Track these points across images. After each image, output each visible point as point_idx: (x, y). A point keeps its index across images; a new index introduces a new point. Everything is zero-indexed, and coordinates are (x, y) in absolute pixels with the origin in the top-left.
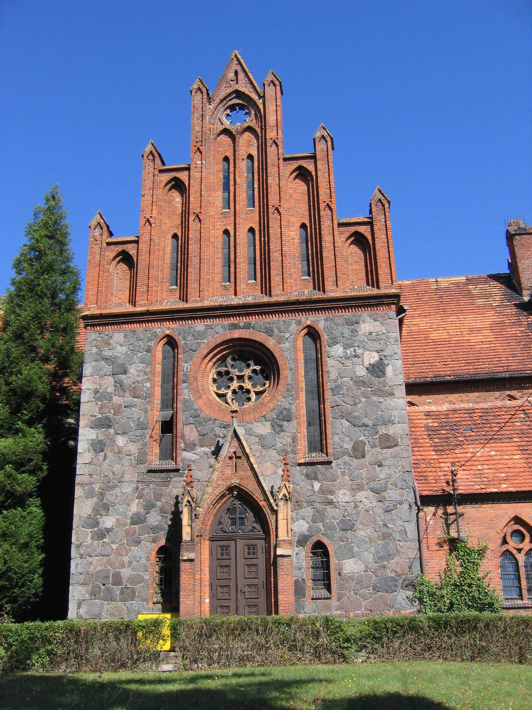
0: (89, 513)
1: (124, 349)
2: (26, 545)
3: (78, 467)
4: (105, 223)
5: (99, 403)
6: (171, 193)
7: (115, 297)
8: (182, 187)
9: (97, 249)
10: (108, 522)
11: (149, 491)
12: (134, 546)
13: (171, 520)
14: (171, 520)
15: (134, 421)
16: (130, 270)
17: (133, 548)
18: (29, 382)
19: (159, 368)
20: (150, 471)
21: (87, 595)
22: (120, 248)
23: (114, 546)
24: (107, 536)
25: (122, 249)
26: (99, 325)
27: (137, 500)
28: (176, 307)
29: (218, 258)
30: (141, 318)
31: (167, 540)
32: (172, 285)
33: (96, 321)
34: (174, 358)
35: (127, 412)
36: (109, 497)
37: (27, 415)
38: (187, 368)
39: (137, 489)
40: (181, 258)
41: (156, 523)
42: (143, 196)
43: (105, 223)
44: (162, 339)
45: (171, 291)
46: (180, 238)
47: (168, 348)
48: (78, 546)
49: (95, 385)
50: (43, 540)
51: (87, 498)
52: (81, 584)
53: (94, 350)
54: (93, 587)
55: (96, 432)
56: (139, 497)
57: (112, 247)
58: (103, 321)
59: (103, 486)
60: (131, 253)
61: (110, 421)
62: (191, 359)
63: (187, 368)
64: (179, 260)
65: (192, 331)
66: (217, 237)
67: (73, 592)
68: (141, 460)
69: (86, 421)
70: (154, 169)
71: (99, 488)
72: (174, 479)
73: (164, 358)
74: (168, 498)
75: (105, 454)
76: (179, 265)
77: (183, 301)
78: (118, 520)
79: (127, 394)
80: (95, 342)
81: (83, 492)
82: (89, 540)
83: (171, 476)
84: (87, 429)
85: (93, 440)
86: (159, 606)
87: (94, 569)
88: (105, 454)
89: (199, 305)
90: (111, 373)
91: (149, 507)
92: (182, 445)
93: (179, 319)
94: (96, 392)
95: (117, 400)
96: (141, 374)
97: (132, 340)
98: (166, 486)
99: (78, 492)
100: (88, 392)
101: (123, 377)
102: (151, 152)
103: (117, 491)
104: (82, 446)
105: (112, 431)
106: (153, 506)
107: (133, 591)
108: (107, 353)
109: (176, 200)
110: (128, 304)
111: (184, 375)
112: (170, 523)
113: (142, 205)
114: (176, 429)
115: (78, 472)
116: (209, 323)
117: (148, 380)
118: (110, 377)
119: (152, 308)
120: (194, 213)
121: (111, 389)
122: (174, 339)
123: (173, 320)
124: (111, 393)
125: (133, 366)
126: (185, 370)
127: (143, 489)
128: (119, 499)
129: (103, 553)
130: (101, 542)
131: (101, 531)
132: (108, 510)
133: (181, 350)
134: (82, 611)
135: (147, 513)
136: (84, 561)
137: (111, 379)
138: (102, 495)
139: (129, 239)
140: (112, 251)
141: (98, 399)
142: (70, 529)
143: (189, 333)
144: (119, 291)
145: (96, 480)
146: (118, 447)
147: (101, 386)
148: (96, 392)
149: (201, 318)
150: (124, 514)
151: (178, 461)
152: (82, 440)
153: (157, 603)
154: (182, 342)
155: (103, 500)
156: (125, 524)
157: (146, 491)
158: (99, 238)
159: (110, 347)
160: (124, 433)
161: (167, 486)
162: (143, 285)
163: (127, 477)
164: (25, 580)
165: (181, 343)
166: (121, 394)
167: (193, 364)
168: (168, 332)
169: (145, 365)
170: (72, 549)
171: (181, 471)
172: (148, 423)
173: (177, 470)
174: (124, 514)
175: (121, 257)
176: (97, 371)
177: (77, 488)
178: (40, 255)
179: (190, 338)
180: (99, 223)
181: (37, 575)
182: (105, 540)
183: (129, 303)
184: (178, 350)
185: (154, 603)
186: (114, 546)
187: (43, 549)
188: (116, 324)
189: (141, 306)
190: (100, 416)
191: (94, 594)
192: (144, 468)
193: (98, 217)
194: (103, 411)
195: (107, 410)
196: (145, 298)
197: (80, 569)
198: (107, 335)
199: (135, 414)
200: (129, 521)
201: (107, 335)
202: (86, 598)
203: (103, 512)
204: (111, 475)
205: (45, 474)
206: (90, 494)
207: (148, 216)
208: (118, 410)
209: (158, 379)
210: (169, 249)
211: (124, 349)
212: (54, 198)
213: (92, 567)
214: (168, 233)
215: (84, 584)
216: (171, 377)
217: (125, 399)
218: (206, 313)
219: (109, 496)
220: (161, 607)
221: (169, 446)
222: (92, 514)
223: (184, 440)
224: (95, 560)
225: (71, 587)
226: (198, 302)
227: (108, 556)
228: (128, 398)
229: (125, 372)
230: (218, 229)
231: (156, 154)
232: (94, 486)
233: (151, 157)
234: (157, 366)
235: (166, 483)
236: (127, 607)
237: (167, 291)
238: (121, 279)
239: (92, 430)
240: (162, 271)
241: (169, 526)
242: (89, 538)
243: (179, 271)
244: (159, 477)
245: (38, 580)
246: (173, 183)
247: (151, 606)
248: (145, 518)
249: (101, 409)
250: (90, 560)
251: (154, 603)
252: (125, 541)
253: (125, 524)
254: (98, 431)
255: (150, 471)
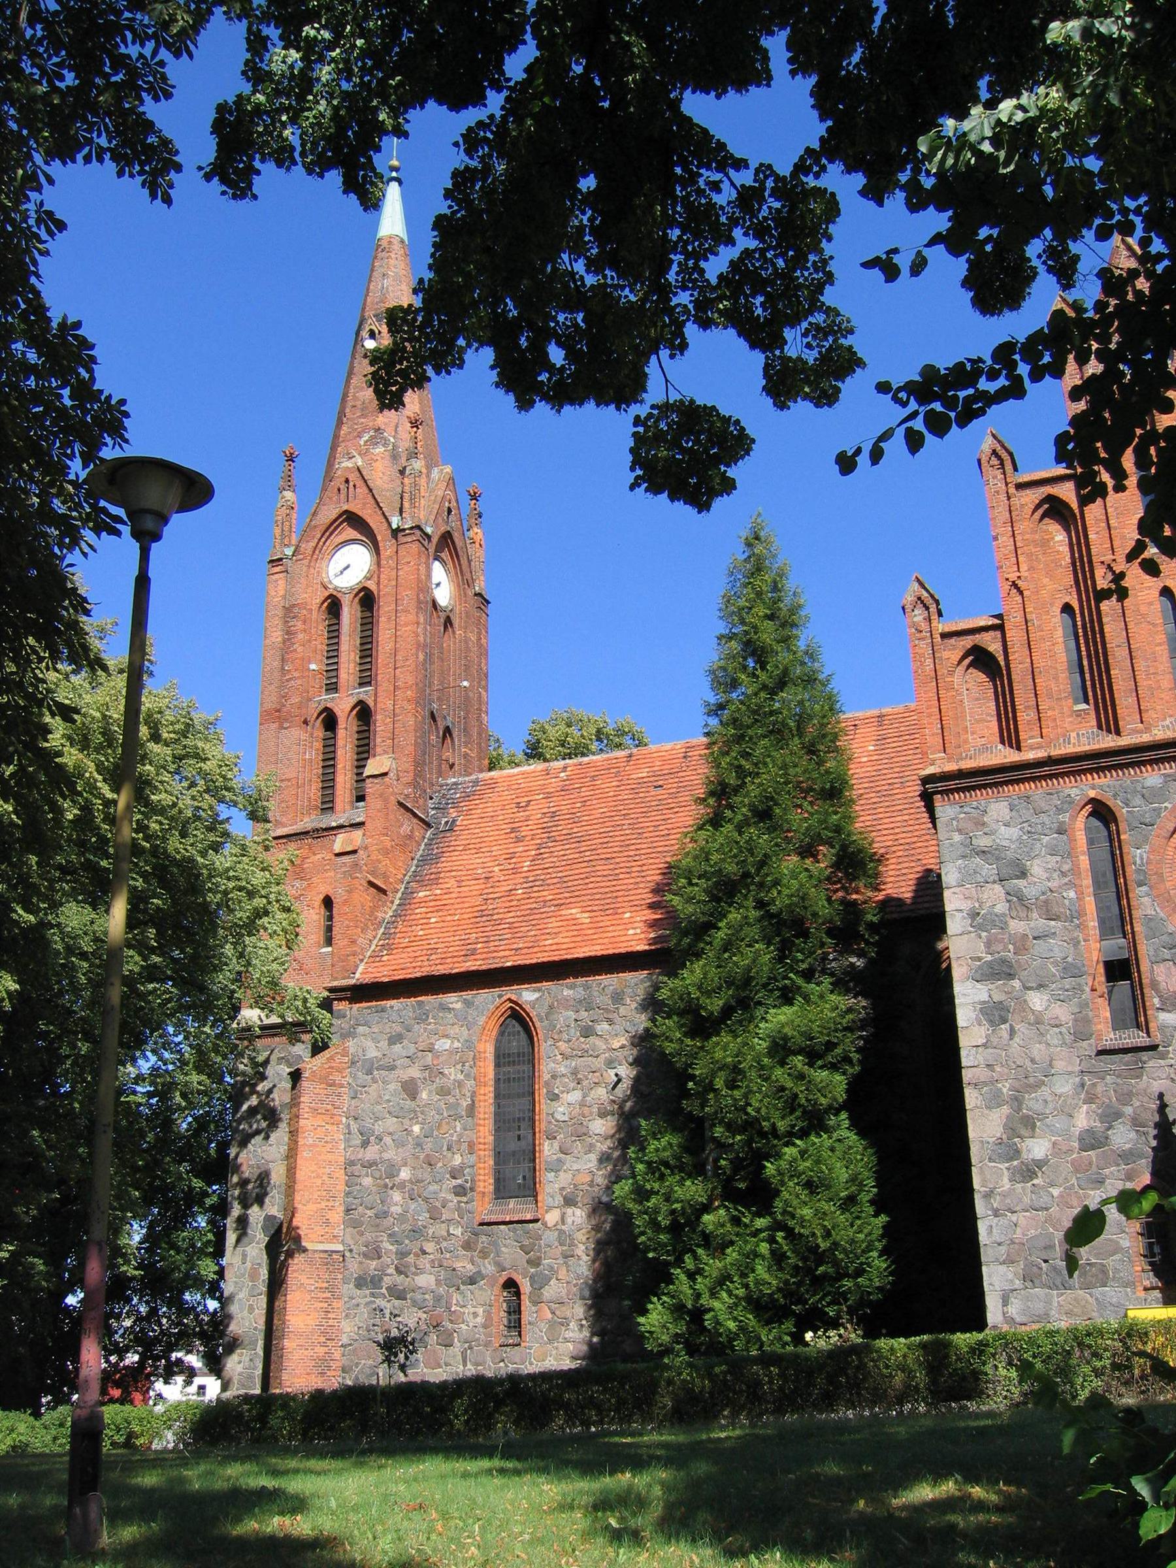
0: (998, 1135)
1: (1014, 832)
2: (851, 1200)
3: (963, 1053)
4: (932, 596)
5: (984, 934)
6: (1043, 526)
7: (973, 733)
8: (1067, 513)
9: (924, 647)
10: (1037, 1148)
11: (1106, 1087)
12: (1092, 1189)
13: (1155, 1137)
14: (1155, 1137)
15: (1056, 964)
16: (993, 680)
17: (1092, 1193)
18: (803, 899)
19: (1084, 861)
20: (1101, 1053)
21: (1017, 1282)
22: (968, 642)
23: (1056, 1192)
24: (1040, 1174)
25: (972, 644)
26: (958, 790)
27: (1085, 1106)
28: (1103, 746)
29: (1160, 644)
30: (1037, 772)
31: (1152, 1174)
32: (1076, 702)
33: (952, 784)
34: (1111, 841)
35: (1040, 947)
36: (1031, 1104)
37: (802, 961)
38: (1142, 859)
39: (1083, 1085)
40: (1088, 650)
41: (1128, 1146)
42: (995, 538)
43: (932, 596)
44: (1084, 807)
45: (1078, 714)
46: (1077, 612)
47: (1096, 823)
48: (988, 1195)
49: (969, 902)
50: (875, 1190)
51: (989, 1108)
52: (1004, 1263)
53: (957, 837)
54: (1025, 1266)
55: (986, 988)
56: (1090, 1100)
57: (953, 641)
58: (965, 782)
59: (1017, 1084)
60: (991, 649)
61: (1011, 967)
62: (1146, 840)
63: (1142, 859)
64: (1084, 653)
65: (1139, 789)
66: (1151, 604)
67: (990, 1276)
68: (1080, 1035)
69: (965, 969)
70: (1007, 484)
71: (1010, 1090)
72: (1151, 1064)
73: (1091, 842)
74: (1146, 1099)
75: (1012, 1028)
76: (1085, 663)
77: (1109, 731)
78: (1054, 1144)
79: (1035, 915)
80: (955, 823)
81: (980, 1098)
82: (1006, 1184)
83: (1144, 1058)
84: (970, 984)
85: (984, 1002)
86: (1157, 1294)
87: (1024, 1235)
88: (1012, 1028)
89: (1146, 738)
90: (997, 878)
91: (1110, 1117)
92: (1156, 1001)
93: (1109, 768)
94: (974, 915)
95: (1017, 926)
96: (1055, 875)
97: (1027, 814)
98: (1137, 1077)
99: (971, 1098)
100: (959, 915)
101: (1021, 883)
102: (994, 452)
103: (1044, 1092)
104: (964, 1016)
105: (1016, 983)
106: (1118, 1115)
107: (1103, 1270)
108: (983, 842)
109: (1057, 539)
110: (1000, 746)
111: (1138, 871)
112: (1154, 1143)
113: (998, 556)
114: (1139, 971)
115: (964, 1062)
116: (1169, 771)
117: (1071, 885)
118: (996, 886)
119: (1056, 752)
120: (1102, 563)
121: (1001, 908)
122: (1107, 806)
123: (1099, 770)
124: (1004, 915)
125: (1037, 861)
126: (1138, 862)
127: (1094, 1085)
128: (1051, 1106)
129: (1037, 1205)
130: (1029, 1184)
131: (1027, 1166)
132: (1034, 1127)
133: (1123, 826)
134: (1013, 1310)
135: (1109, 1129)
136: (1003, 1221)
137: (997, 888)
138: (1017, 1101)
139: (982, 623)
140: (954, 648)
141: (980, 927)
142: (968, 1164)
143: (1135, 791)
144: (978, 721)
145: (1001, 1074)
146: (1033, 1011)
147: (981, 904)
148: (974, 915)
149: (1151, 762)
150: (1067, 1134)
151: (1151, 1030)
152: (962, 1004)
153: (1153, 1288)
154: (1124, 811)
155: (1020, 1110)
156: (1070, 1151)
157: (1100, 1089)
158: (924, 626)
159: (986, 830)
160: (1041, 986)
161: (1139, 1077)
162: (1027, 708)
163: (1060, 1065)
164: (862, 1264)
165: (1122, 812)
166: (1023, 914)
167: (1152, 851)
168: (1092, 794)
169: (1059, 858)
170: (976, 1202)
171: (1160, 1048)
172: (1084, 965)
173: (1153, 1048)
174: (1067, 1134)
175: (971, 658)
176: (968, 877)
177: (968, 1092)
178: (755, 651)
179: (1138, 800)
180: (919, 598)
181: (875, 1254)
182: (1035, 1181)
183: (1003, 742)
184: (1117, 826)
185: (1146, 1289)
186: (1056, 1192)
187: (879, 1205)
188: (990, 785)
189: (1032, 749)
190: (989, 958)
191: (1029, 1278)
192: (1088, 1047)
193: (916, 585)
194: (993, 948)
195: (1000, 947)
196: (1037, 732)
197: (997, 1236)
198: (977, 808)
199: (1056, 949)
200: (1076, 1145)
201: (977, 808)
202: (1016, 1287)
203: (1024, 1132)
204: (1028, 1063)
205: (857, 1068)
206: (995, 1101)
207: (1013, 576)
208: (1021, 944)
209: (1087, 881)
210: (1059, 633)
211: (1014, 832)
212: (757, 538)
213: (1018, 1230)
214: (1052, 604)
215: (1009, 1261)
216: (1110, 876)
217: (1032, 924)
218: (1161, 753)
219: (1032, 1103)
220: (1160, 1295)
221: (1129, 1003)
222: (1004, 1137)
223: (1157, 991)
224: (1022, 1218)
225: (984, 1269)
226: (1141, 732)
227: (1047, 1209)
228: (1039, 922)
229: (1023, 874)
230: (1150, 588)
231: (1004, 455)
232: (1000, 1085)
233: (995, 461)
234: (1082, 858)
235: (1138, 1071)
236: (1097, 1299)
237: (1071, 716)
238: (977, 699)
239: (978, 985)
240: (1056, 678)
241: (1153, 1149)
242: (1006, 1180)
243: (1087, 676)
244: (1121, 1061)
245: (878, 1263)
246: (1046, 506)
247: (1142, 1294)
248: (1107, 1138)
249: (988, 944)
250: (1014, 1218)
251: (1146, 1289)
252: (1074, 1181)
253: (1070, 1151)
254: (991, 986)
255: (1101, 1053)
